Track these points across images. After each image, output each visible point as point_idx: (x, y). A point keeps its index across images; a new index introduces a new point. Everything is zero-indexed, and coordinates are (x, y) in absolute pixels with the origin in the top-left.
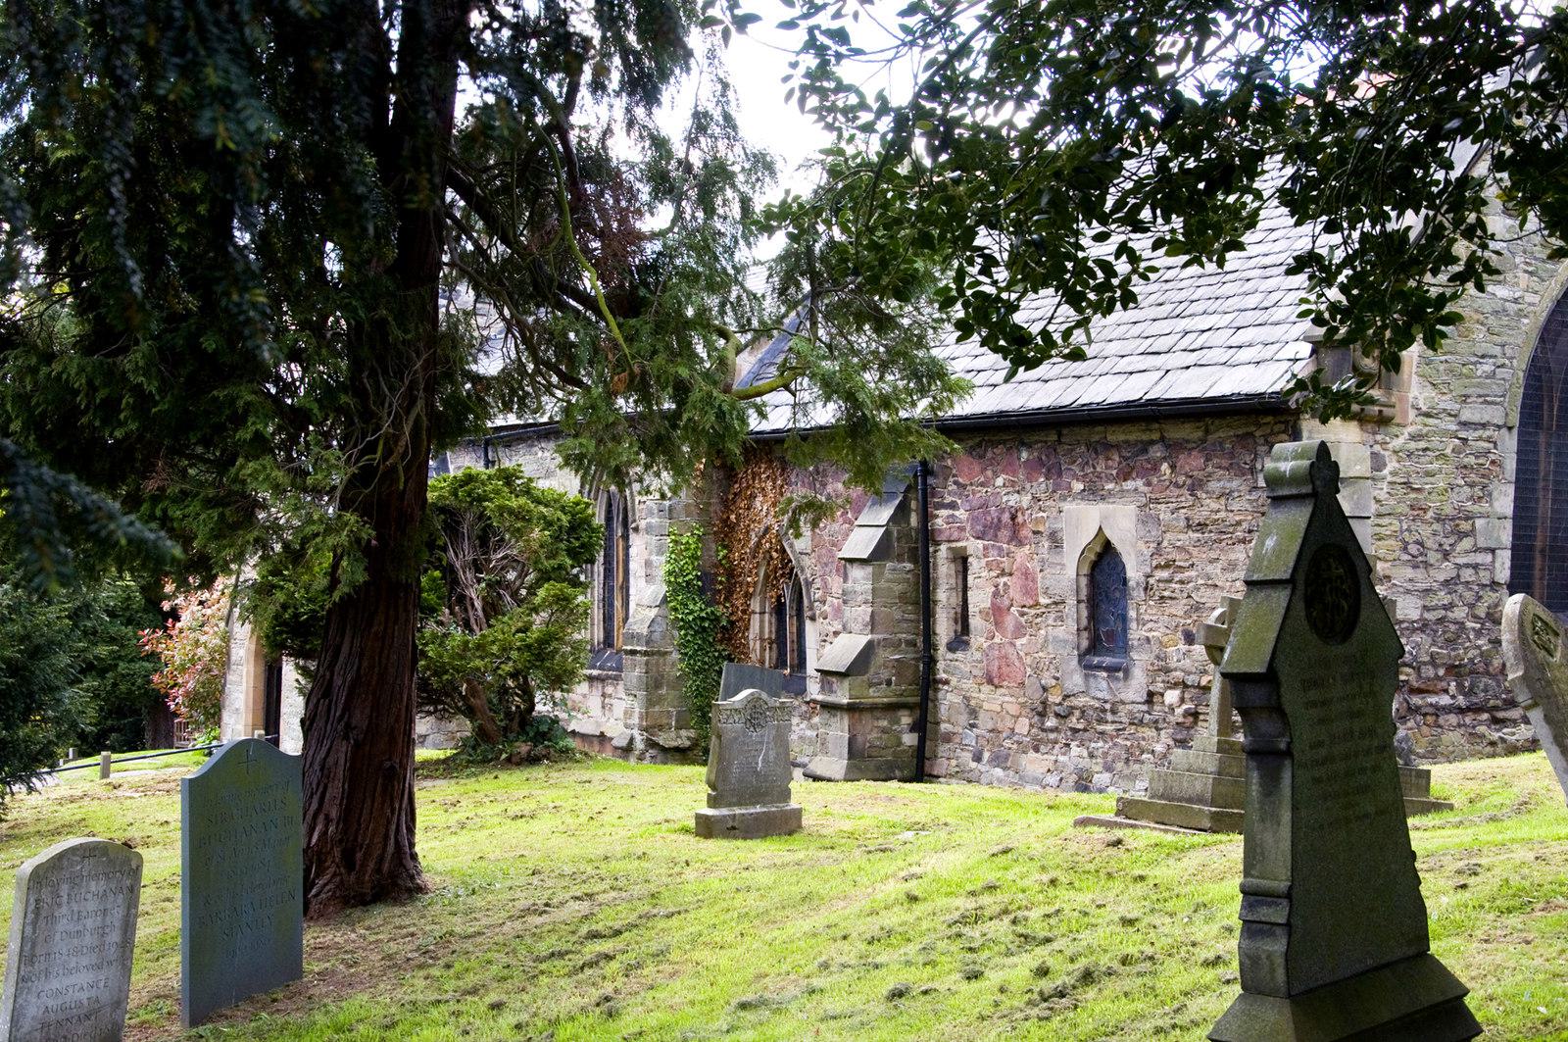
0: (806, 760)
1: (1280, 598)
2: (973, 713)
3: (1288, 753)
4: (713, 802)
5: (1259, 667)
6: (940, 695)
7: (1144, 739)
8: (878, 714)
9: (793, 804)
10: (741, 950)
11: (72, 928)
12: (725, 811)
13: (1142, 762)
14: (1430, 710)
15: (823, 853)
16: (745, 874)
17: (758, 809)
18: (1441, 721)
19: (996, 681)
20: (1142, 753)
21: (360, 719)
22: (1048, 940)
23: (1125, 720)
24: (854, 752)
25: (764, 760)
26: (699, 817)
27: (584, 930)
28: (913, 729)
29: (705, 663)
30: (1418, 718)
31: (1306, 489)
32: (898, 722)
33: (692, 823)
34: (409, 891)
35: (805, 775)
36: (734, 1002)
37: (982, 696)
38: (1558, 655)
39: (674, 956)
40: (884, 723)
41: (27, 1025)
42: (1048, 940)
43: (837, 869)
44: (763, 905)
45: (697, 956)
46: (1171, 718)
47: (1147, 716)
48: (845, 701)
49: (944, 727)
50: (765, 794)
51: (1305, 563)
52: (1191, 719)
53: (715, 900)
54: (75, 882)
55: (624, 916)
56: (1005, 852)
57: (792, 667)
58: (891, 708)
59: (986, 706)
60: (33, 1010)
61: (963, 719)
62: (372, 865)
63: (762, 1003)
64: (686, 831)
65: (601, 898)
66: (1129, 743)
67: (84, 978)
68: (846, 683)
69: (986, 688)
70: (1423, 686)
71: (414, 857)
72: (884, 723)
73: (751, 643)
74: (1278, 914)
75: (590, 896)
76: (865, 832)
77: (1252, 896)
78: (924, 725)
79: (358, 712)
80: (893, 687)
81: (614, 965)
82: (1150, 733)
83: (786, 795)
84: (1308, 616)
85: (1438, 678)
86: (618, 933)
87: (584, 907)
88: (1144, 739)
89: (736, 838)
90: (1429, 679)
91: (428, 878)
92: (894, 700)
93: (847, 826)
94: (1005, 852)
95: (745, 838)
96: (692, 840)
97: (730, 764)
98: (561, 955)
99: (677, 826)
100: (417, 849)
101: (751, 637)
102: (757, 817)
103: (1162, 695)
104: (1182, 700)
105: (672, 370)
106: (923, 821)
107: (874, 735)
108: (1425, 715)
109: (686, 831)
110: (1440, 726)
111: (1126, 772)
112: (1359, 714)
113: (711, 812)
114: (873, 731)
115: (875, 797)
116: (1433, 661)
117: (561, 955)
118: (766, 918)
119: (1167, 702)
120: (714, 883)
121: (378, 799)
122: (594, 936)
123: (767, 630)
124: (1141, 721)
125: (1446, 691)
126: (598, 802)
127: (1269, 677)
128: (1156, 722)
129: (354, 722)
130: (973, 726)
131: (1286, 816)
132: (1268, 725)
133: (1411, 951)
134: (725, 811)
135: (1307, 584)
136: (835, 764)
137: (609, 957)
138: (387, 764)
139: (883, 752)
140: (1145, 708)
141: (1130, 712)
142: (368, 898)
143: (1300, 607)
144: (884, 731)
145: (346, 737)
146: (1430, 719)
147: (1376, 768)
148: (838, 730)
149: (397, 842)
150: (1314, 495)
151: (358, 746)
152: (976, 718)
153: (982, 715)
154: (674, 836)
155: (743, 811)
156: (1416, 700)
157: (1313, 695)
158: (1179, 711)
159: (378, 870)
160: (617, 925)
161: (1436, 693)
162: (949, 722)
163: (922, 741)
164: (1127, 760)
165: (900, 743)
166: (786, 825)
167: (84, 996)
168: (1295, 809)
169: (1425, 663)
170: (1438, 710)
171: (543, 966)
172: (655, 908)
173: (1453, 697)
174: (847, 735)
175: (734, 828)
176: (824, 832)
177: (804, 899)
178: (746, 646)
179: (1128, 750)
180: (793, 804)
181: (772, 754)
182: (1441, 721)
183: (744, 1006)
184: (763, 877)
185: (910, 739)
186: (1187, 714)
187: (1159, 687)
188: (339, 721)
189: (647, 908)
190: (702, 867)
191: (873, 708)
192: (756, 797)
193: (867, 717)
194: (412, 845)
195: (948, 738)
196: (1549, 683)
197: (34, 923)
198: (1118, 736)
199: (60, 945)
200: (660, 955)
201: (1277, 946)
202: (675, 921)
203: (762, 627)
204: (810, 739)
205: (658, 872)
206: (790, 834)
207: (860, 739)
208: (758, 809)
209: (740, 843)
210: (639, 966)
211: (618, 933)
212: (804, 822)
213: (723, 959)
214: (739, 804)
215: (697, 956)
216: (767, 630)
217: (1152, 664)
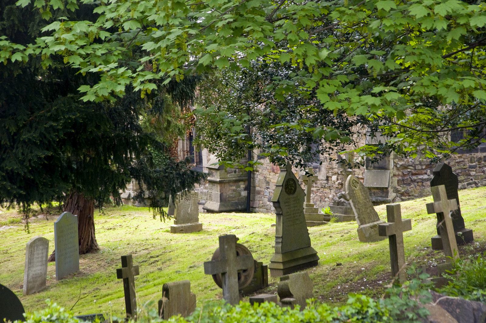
0: (204, 202)
1: (281, 188)
2: (268, 183)
3: (282, 214)
4: (176, 223)
5: (276, 200)
6: (256, 176)
7: (326, 193)
8: (231, 184)
9: (200, 222)
10: (189, 258)
11: (37, 256)
12: (179, 225)
13: (325, 202)
14: (420, 180)
15: (208, 236)
16: (188, 242)
17: (189, 224)
18: (424, 184)
19: (275, 171)
20: (325, 198)
21: (81, 204)
22: (256, 252)
23: (320, 186)
24: (222, 199)
25: (190, 210)
26: (172, 227)
27: (149, 256)
28: (245, 189)
29: (160, 162)
30: (415, 183)
31: (285, 170)
32: (239, 187)
33: (170, 229)
34: (96, 250)
35: (204, 209)
36: (189, 267)
37: (271, 177)
38: (358, 188)
39: (173, 260)
40: (234, 188)
41: (30, 277)
42: (256, 252)
43: (211, 239)
44: (193, 249)
45: (179, 259)
46: (335, 186)
47: (327, 185)
48: (218, 180)
49: (257, 188)
50: (191, 220)
51: (285, 183)
52: (340, 186)
53: (181, 248)
54: (37, 246)
55: (157, 253)
56: (253, 233)
57: (196, 163)
58: (237, 181)
59: (272, 180)
60: (31, 275)
61: (264, 185)
62: (86, 243)
63: (194, 266)
64: (168, 231)
65: (150, 249)
66: (321, 195)
67: (39, 268)
68: (218, 172)
69: (272, 174)
70: (417, 173)
71: (96, 241)
72: (234, 188)
73: (179, 153)
74: (280, 240)
75: (147, 249)
76: (221, 230)
77: (277, 238)
78: (249, 188)
79: (81, 203)
80: (237, 173)
81: (159, 263)
82: (327, 191)
83: (197, 220)
84: (286, 191)
85: (422, 169)
86: (158, 256)
87: (146, 251)
88: (326, 193)
89: (183, 233)
90: (419, 170)
91: (100, 247)
92: (237, 178)
93: (216, 228)
94: (253, 233)
95: (186, 233)
96: (171, 234)
97: (180, 211)
98: (145, 261)
99: (165, 230)
100: (96, 239)
101: (179, 150)
102: (189, 227)
103: (331, 177)
104: (338, 179)
105: (166, 118)
106: (239, 226)
107: (230, 192)
108: (418, 182)
109: (168, 231)
110: (423, 186)
111: (320, 205)
112: (296, 207)
113: (175, 226)
114: (230, 190)
115: (225, 219)
116: (420, 164)
117: (145, 261)
118: (194, 251)
119: (333, 180)
120: (180, 244)
121: (87, 227)
122: (152, 257)
123: (185, 147)
124: (325, 187)
125: (426, 174)
126: (135, 223)
127: (278, 202)
128: (330, 187)
129: (80, 205)
130: (268, 188)
131: (282, 224)
132: (279, 210)
133: (308, 246)
134: (179, 225)
135: (285, 186)
136: (215, 205)
137: (157, 261)
138: (89, 216)
139: (234, 199)
140: (326, 182)
141: (321, 184)
142: (85, 252)
143: (284, 189)
144: (234, 190)
145: (78, 209)
146: (420, 184)
147: (300, 215)
148: (216, 191)
149: (91, 237)
150: (287, 170)
151: (81, 211)
152: (269, 185)
153: (271, 184)
154: (165, 233)
155: (185, 225)
156: (414, 178)
157: (287, 204)
158: (337, 183)
159: (87, 245)
160: (157, 255)
161: (422, 174)
162: (259, 186)
163: (249, 194)
164: (321, 201)
165: (240, 195)
166: (198, 229)
167: (39, 272)
168: (283, 223)
169: (417, 165)
170: (423, 180)
171: (142, 264)
172: (165, 250)
173: (429, 175)
174: (219, 193)
175: (182, 230)
176: (209, 230)
177: (203, 247)
178: (177, 153)
179: (321, 197)
180: (200, 222)
181: (193, 208)
182: (424, 184)
183: (191, 267)
184: (193, 243)
185: (244, 194)
186: (339, 184)
187: (330, 174)
188: (76, 205)
189: (164, 251)
190: (175, 241)
191: (229, 182)
192: (189, 220)
193: (227, 186)
194: (95, 237)
195: (259, 192)
196: (354, 194)
197: (31, 255)
198: (317, 192)
199: (35, 260)
200: (170, 260)
201: (280, 245)
202: (172, 253)
203: (183, 146)
204: (205, 193)
205: (165, 244)
206: (199, 231)
207: (224, 194)
208: (189, 224)
209: (184, 234)
210: (165, 262)
211: (158, 256)
212: (203, 228)
213: (185, 260)
214: (183, 223)
215: (179, 259)
216: (185, 147)
217: (328, 166)
